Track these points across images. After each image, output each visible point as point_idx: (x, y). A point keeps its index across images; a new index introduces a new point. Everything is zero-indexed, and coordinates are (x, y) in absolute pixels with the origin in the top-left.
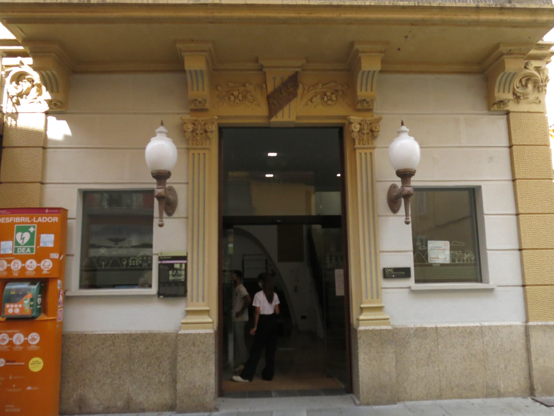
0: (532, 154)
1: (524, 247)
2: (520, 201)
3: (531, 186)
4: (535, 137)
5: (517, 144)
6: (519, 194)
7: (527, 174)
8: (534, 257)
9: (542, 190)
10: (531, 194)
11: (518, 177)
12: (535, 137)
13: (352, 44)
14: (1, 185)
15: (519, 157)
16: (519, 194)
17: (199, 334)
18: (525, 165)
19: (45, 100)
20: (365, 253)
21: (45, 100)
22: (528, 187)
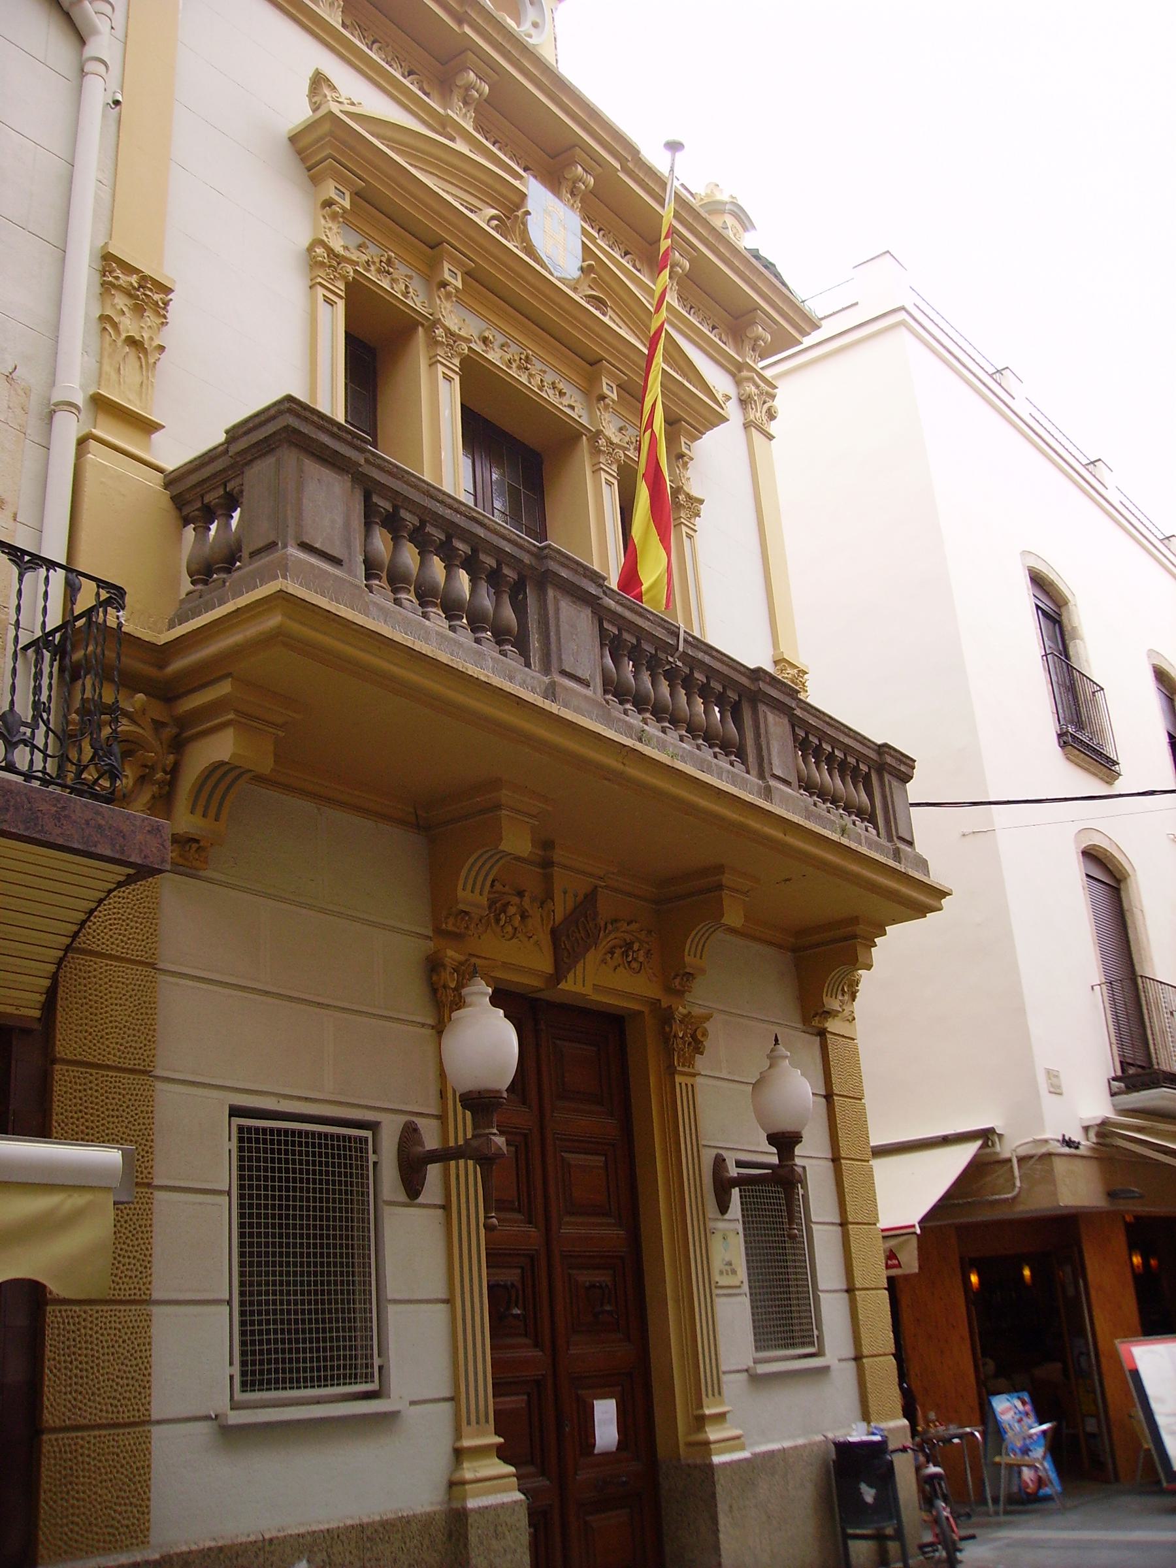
0: (102, 1335)
1: (47, 1421)
2: (52, 1383)
3: (89, 1325)
4: (113, 1522)
5: (70, 1057)
6: (51, 1355)
7: (80, 1409)
8: (85, 1090)
9: (118, 1465)
10: (92, 1115)
11: (51, 1422)
12: (113, 1522)
13: (525, 891)
14: (477, 1559)
15: (61, 1346)
16: (51, 1355)
17: (503, 1505)
18: (76, 1376)
19: (164, 427)
20: (707, 1390)
21: (164, 427)
22: (85, 1090)
